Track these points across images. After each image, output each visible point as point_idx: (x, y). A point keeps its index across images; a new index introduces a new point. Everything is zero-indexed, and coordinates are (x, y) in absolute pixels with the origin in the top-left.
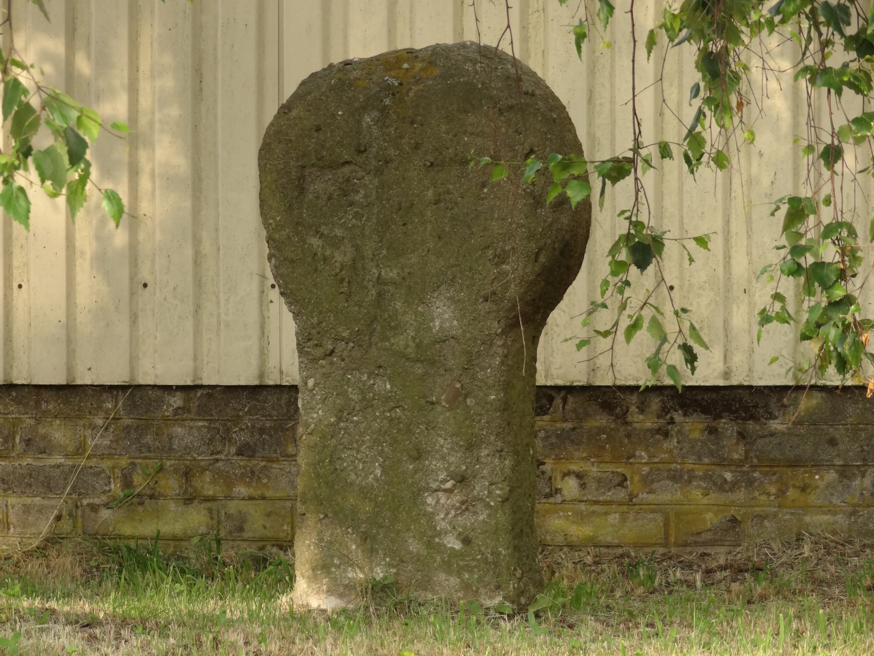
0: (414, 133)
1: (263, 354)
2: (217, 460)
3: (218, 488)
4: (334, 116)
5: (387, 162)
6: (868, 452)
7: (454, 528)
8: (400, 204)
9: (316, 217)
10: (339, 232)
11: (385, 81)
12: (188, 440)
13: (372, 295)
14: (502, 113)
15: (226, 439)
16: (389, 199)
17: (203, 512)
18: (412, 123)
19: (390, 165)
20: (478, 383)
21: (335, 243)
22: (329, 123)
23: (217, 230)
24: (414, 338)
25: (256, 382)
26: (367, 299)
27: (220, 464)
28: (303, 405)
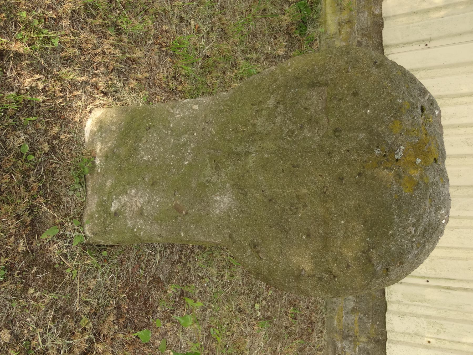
0: (351, 177)
1: (396, 45)
2: (355, 33)
3: (344, 35)
4: (367, 106)
5: (329, 154)
6: (361, 299)
7: (123, 207)
8: (298, 166)
9: (292, 99)
10: (279, 119)
11: (399, 146)
12: (363, 19)
13: (236, 149)
14: (364, 253)
15: (364, 36)
16: (302, 156)
17: (335, 31)
18: (359, 174)
19: (327, 156)
20: (188, 226)
21: (271, 118)
22: (359, 103)
23: (452, 15)
24: (209, 181)
25: (384, 44)
26: (233, 145)
27: (353, 34)
28: (185, 103)
